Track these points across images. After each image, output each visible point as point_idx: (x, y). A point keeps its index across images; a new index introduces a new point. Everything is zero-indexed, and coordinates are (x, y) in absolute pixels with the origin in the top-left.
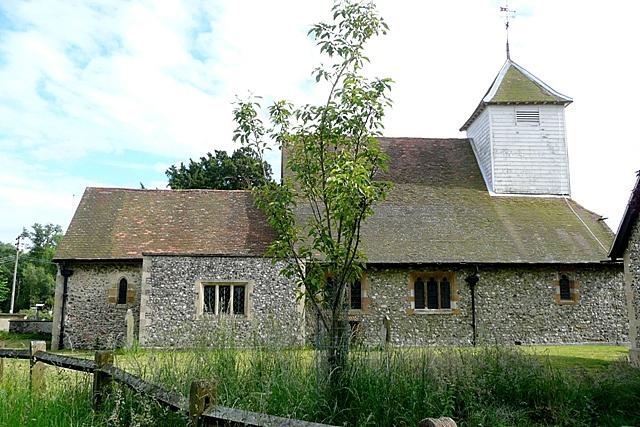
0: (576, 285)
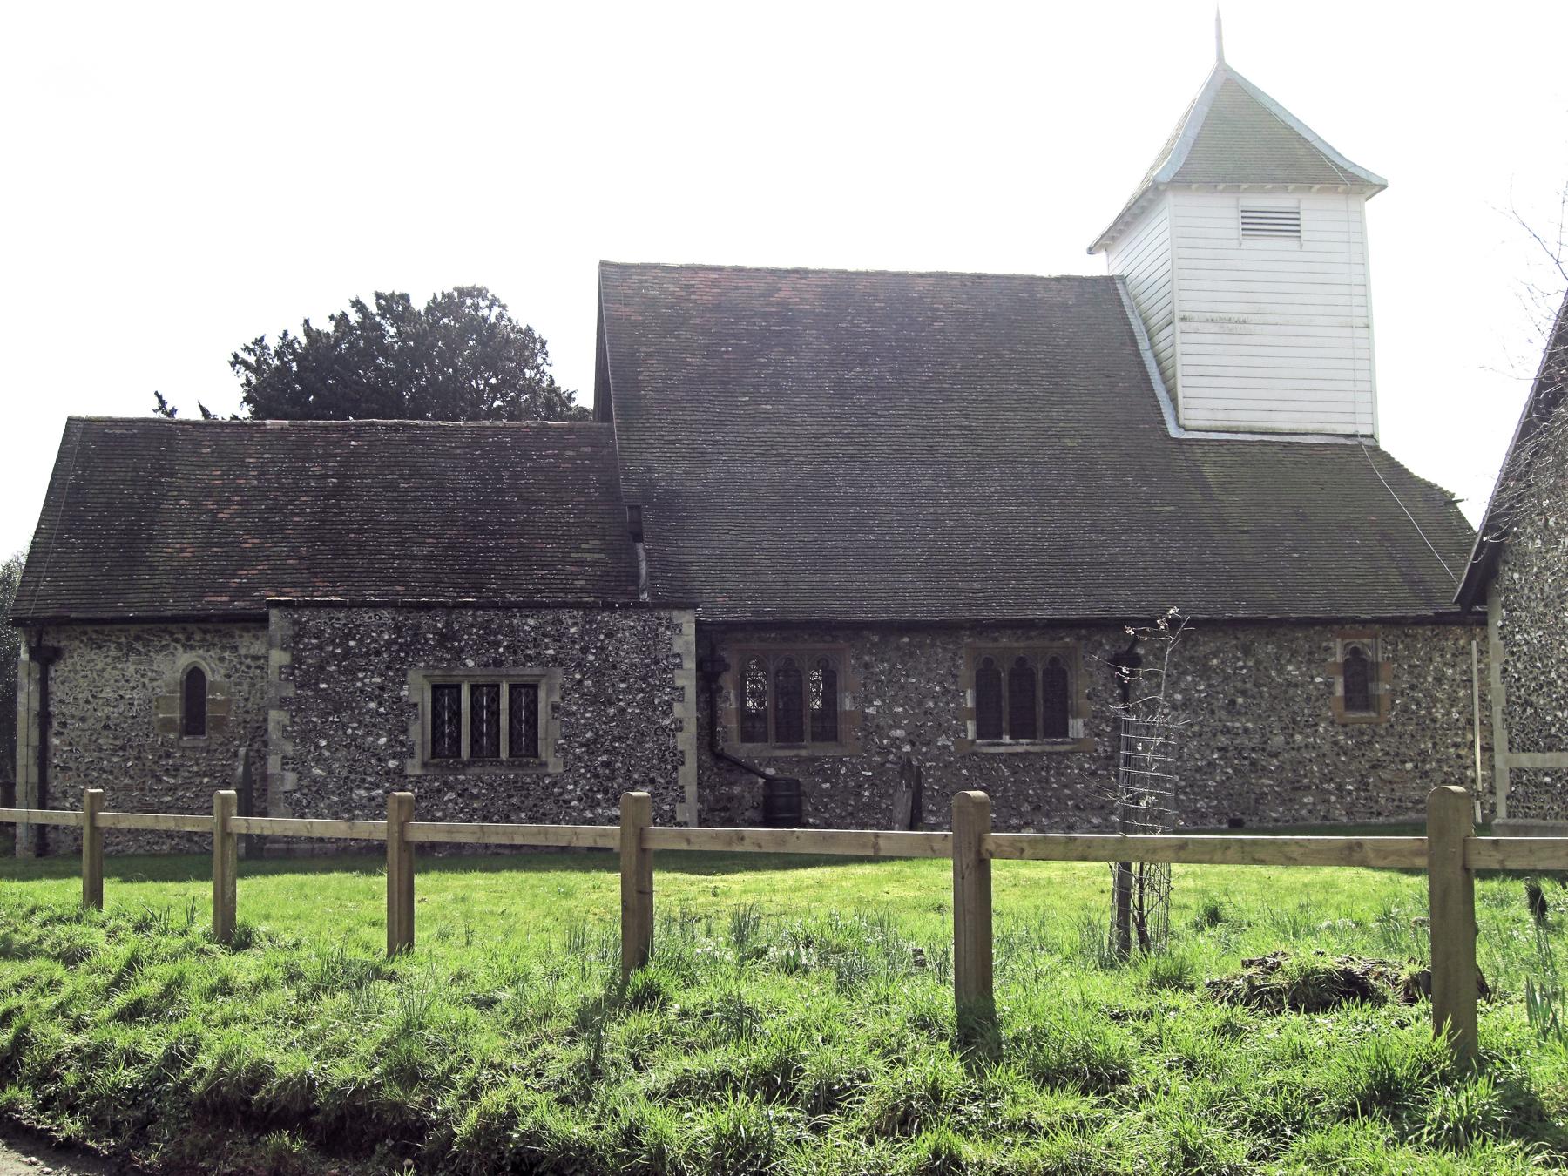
0: (1383, 674)
